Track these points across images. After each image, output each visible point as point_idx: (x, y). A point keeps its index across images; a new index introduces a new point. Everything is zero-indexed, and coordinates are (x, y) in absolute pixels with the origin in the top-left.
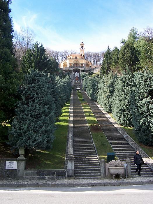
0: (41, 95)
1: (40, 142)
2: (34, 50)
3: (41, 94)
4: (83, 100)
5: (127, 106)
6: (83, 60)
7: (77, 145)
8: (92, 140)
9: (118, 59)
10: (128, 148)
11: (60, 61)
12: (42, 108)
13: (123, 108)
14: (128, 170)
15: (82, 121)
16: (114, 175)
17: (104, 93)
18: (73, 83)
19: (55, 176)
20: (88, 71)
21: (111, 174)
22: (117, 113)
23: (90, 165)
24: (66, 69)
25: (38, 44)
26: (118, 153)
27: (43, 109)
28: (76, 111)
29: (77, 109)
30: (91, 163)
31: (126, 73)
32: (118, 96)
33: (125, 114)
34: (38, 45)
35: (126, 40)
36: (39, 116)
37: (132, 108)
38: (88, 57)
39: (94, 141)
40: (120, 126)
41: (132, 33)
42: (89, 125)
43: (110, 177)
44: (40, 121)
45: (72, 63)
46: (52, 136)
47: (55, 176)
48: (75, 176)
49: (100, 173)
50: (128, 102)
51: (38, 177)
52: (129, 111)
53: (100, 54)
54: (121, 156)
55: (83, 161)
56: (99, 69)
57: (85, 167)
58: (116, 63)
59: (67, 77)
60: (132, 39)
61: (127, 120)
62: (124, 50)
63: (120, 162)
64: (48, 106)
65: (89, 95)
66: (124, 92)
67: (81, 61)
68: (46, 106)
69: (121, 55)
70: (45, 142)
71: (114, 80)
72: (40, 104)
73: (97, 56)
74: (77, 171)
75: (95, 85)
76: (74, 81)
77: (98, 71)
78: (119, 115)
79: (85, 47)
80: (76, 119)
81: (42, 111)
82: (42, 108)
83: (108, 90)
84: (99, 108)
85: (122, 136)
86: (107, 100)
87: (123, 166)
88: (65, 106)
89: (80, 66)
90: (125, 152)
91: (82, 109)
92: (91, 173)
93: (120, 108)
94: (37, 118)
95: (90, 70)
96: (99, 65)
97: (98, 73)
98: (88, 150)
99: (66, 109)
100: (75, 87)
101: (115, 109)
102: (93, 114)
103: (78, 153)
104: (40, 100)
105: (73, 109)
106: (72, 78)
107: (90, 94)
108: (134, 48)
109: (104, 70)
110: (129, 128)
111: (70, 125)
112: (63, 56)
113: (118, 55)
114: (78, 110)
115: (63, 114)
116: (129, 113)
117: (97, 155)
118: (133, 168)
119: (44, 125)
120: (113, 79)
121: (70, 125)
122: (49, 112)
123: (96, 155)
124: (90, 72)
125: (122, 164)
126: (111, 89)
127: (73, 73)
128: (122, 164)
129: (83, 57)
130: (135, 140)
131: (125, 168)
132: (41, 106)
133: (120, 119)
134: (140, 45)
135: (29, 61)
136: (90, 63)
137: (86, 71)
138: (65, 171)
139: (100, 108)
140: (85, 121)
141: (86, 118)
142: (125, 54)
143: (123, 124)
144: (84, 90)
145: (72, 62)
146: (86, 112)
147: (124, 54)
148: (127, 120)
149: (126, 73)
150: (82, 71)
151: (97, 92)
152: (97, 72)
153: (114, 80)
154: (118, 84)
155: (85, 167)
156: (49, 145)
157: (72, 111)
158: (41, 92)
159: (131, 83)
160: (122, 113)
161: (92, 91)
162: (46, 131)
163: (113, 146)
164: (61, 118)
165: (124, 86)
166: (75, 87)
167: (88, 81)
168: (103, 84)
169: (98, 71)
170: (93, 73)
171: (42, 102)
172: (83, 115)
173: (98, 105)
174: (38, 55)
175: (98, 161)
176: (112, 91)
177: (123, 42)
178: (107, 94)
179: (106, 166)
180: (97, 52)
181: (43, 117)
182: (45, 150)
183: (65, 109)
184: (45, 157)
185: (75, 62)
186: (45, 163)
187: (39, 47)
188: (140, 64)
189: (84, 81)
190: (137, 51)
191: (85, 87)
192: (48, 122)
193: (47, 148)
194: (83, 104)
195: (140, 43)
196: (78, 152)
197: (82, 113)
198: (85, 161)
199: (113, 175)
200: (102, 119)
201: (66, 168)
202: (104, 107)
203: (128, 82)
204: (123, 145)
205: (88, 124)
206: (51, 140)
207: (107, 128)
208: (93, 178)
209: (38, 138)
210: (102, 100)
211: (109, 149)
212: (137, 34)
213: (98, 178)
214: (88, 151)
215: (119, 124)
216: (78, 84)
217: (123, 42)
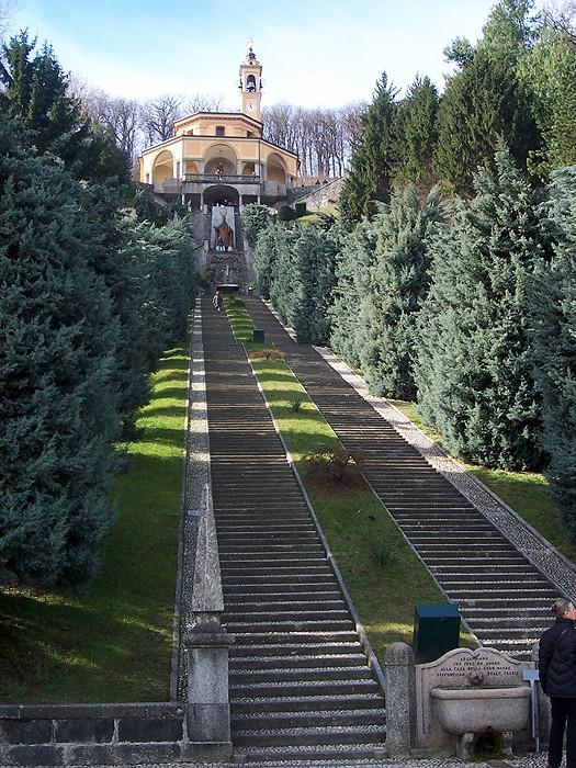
0: (34, 265)
1: (26, 542)
3: (34, 257)
4: (259, 337)
5: (502, 356)
7: (237, 565)
8: (317, 534)
9: (435, 137)
10: (523, 578)
11: (138, 149)
12: (42, 338)
13: (478, 368)
15: (254, 436)
16: (469, 737)
17: (370, 297)
18: (203, 257)
19: (115, 742)
20: (279, 199)
21: (446, 730)
22: (449, 394)
23: (321, 677)
24: (169, 185)
25: (29, 43)
26: (466, 605)
27: (46, 344)
28: (223, 387)
29: (227, 379)
30: (324, 663)
31: (496, 182)
32: (454, 307)
33: (489, 401)
34: (28, 49)
35: (474, 44)
36: (24, 383)
37: (539, 364)
38: (276, 130)
40: (462, 467)
41: (507, 10)
42: (298, 457)
43: (443, 747)
44: (30, 413)
45: (200, 156)
46: (96, 507)
47: (115, 742)
48: (237, 743)
49: (381, 721)
50: (507, 339)
51: (12, 752)
52: (514, 384)
53: (339, 117)
55: (274, 652)
56: (335, 191)
57: (290, 684)
58: (425, 156)
59: (177, 222)
60: (504, 41)
61: (500, 430)
62: (466, 91)
63: (497, 659)
64: (76, 329)
65: (284, 317)
66: (488, 285)
67: (247, 151)
68: (64, 329)
70: (57, 538)
71: (423, 230)
72: (28, 315)
73: (321, 130)
74: (248, 709)
75: (319, 267)
76: (207, 248)
77: (331, 201)
78: (456, 404)
79: (266, 77)
80: (225, 427)
81: (42, 354)
82: (42, 338)
83: (389, 282)
84: (343, 376)
85: (481, 516)
86: (385, 334)
88: (167, 365)
89: (240, 172)
90: (509, 605)
92: (328, 722)
93: (465, 371)
94: (13, 398)
95: (289, 196)
96: (331, 175)
97: (334, 211)
98: (297, 589)
99: (169, 378)
100: (214, 274)
101: (435, 377)
102: (312, 406)
104: (28, 294)
105: (207, 379)
106: (200, 233)
107: (290, 312)
108: (517, 85)
109: (360, 194)
110: (511, 475)
111: (193, 455)
113: (433, 118)
115: (156, 404)
116: (514, 394)
117: (356, 617)
119: (50, 436)
120: (418, 226)
121: (193, 455)
122: (83, 367)
123: (349, 616)
124: (290, 203)
126: (408, 273)
127: (204, 208)
130: (551, 539)
131: (528, 697)
132: (34, 325)
134: (540, 71)
136: (291, 163)
139: (348, 378)
140: (273, 436)
141: (279, 425)
142: (471, 110)
143: (482, 454)
144: (257, 293)
145: (201, 151)
146: (273, 395)
148: (500, 430)
149: (496, 182)
150: (249, 199)
151: (328, 296)
152: (322, 204)
153: (423, 230)
154: (454, 244)
155: (290, 684)
156: (82, 556)
157: (200, 387)
158: (38, 245)
159: (523, 239)
161: (301, 295)
162: (62, 475)
163: (438, 570)
165: (486, 254)
167: (282, 247)
168: (362, 255)
169: (331, 201)
170: (302, 210)
171: (40, 306)
172: (258, 410)
173: (332, 360)
174: (26, 99)
175: (361, 650)
176: (417, 288)
177: (459, 54)
178: (387, 302)
179: (418, 683)
180: (323, 111)
181: (46, 390)
182: (57, 587)
183: (161, 380)
184: (53, 632)
185: (215, 154)
186: (58, 667)
187: (31, 58)
188: (547, 160)
189: (261, 247)
190: (531, 97)
191: (267, 276)
192: (78, 420)
193: (71, 578)
195: (546, 61)
196: (245, 599)
198: (287, 652)
199: (461, 736)
200: (362, 429)
201: (181, 696)
202: (368, 369)
203: (505, 234)
204: (492, 562)
205: (291, 452)
206: (93, 528)
207: (395, 473)
208: (343, 756)
209: (13, 515)
210: (359, 334)
212: (532, 13)
213: (370, 755)
214: (302, 598)
215: (455, 454)
216: (231, 260)
217: (459, 54)
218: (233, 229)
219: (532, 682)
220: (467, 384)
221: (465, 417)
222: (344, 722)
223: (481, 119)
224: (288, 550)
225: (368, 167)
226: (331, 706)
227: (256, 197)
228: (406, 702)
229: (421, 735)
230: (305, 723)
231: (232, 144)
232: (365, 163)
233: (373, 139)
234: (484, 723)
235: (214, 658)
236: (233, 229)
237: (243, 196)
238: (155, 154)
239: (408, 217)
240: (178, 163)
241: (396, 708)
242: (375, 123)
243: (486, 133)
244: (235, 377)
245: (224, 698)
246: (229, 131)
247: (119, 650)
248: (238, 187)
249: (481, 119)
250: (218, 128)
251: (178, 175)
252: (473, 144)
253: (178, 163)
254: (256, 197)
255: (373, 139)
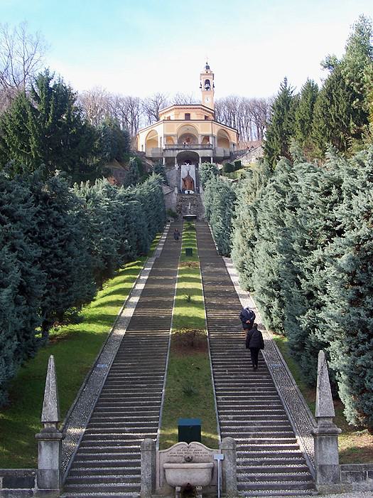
2: (37, 98)
6: (208, 124)
14: (225, 472)
15: (158, 319)
16: (178, 489)
20: (225, 158)
21: (171, 486)
25: (50, 76)
34: (49, 80)
35: (340, 58)
39: (166, 386)
41: (358, 36)
45: (175, 133)
49: (138, 480)
54: (235, 430)
58: (306, 131)
63: (200, 448)
67: (205, 129)
69: (319, 107)
73: (256, 108)
76: (176, 191)
78: (265, 299)
79: (215, 82)
87: (210, 460)
89: (200, 143)
91: (174, 281)
92: (119, 481)
95: (231, 156)
98: (137, 410)
99: (125, 281)
100: (181, 209)
103: (103, 421)
112: (150, 112)
113: (312, 106)
114: (159, 286)
118: (258, 467)
124: (232, 161)
125: (209, 453)
127: (176, 166)
128: (209, 453)
129: (212, 115)
130: (298, 380)
133: (268, 313)
135: (21, 133)
137: (217, 160)
138: (30, 472)
142: (332, 102)
145: (175, 129)
147: (328, 103)
150: (206, 159)
160: (276, 293)
164: (86, 311)
166: (180, 211)
170: (239, 166)
174: (48, 110)
178: (249, 234)
179: (157, 460)
185: (183, 131)
187: (51, 85)
194: (183, 266)
197: (170, 293)
211: (204, 406)
218: (195, 180)
219: (219, 460)
220: (271, 287)
221: (269, 307)
222: (126, 481)
223: (338, 108)
224: (143, 387)
225: (275, 138)
226: (124, 472)
227: (210, 158)
228: (150, 470)
229: (158, 488)
230: (106, 481)
231: (195, 124)
232: (273, 135)
233: (278, 120)
234: (184, 481)
235: (52, 446)
236: (195, 180)
237: (202, 158)
238: (147, 132)
239: (263, 180)
240: (161, 138)
241: (146, 474)
242: (279, 110)
243: (341, 117)
244: (165, 279)
245: (56, 467)
246: (193, 116)
247: (23, 442)
248: (198, 152)
249: (338, 108)
250: (186, 114)
251: (161, 145)
252: (333, 124)
253: (161, 138)
254: (210, 158)
255: (278, 120)
